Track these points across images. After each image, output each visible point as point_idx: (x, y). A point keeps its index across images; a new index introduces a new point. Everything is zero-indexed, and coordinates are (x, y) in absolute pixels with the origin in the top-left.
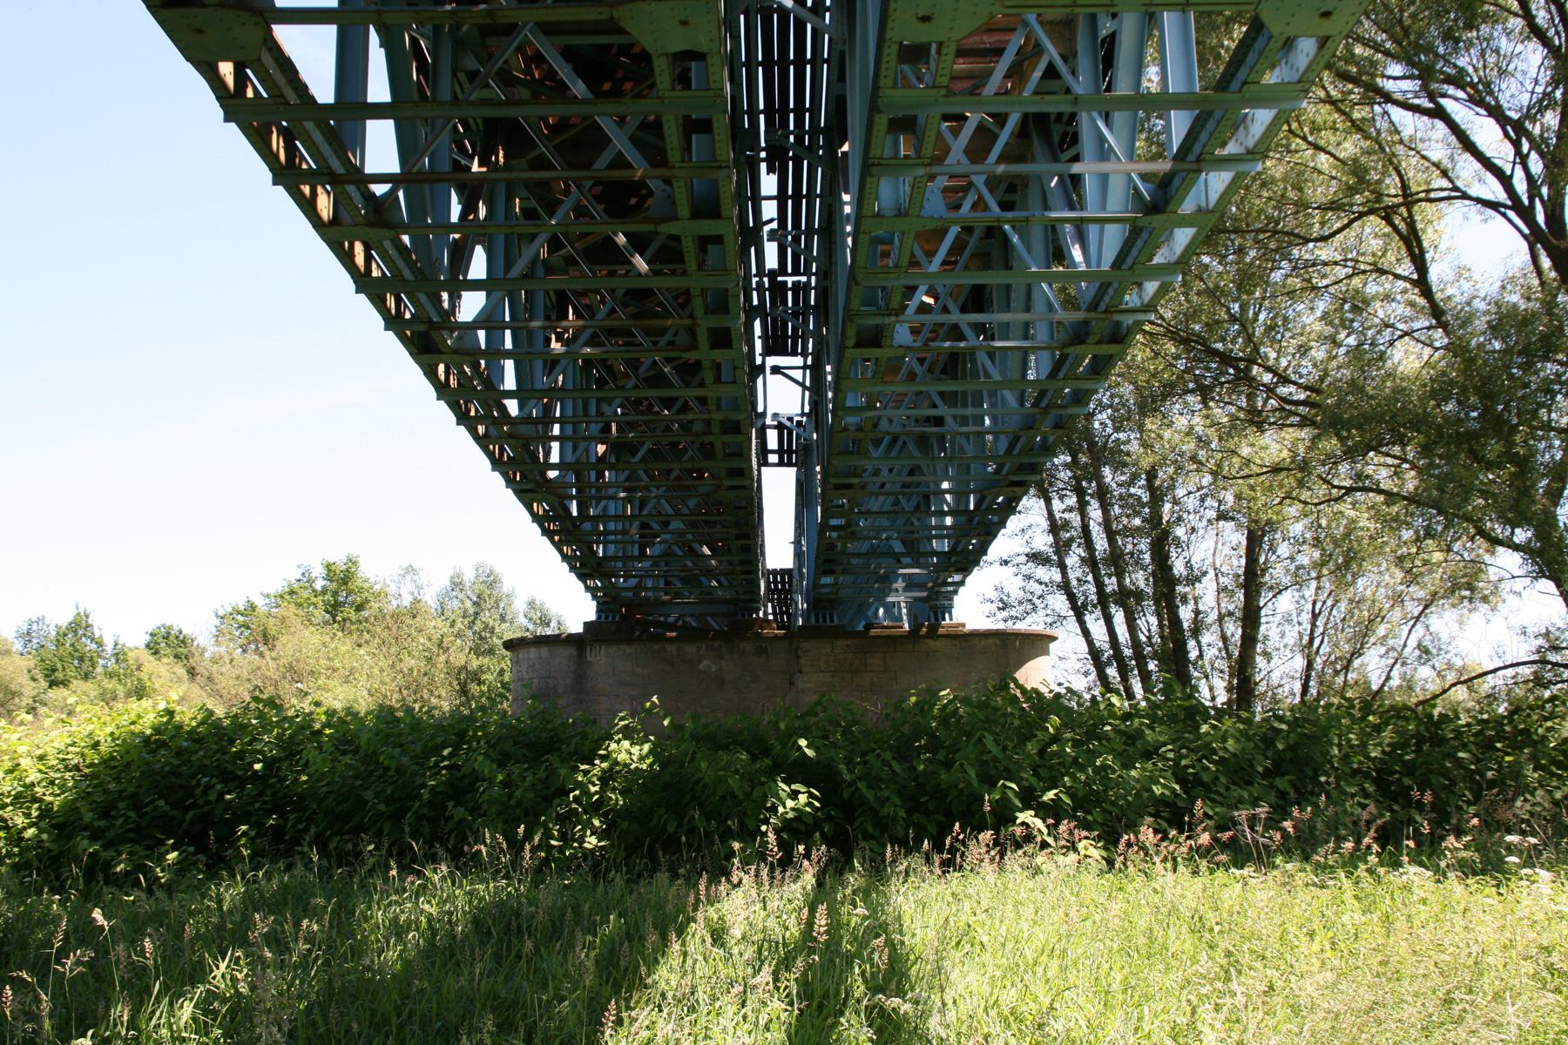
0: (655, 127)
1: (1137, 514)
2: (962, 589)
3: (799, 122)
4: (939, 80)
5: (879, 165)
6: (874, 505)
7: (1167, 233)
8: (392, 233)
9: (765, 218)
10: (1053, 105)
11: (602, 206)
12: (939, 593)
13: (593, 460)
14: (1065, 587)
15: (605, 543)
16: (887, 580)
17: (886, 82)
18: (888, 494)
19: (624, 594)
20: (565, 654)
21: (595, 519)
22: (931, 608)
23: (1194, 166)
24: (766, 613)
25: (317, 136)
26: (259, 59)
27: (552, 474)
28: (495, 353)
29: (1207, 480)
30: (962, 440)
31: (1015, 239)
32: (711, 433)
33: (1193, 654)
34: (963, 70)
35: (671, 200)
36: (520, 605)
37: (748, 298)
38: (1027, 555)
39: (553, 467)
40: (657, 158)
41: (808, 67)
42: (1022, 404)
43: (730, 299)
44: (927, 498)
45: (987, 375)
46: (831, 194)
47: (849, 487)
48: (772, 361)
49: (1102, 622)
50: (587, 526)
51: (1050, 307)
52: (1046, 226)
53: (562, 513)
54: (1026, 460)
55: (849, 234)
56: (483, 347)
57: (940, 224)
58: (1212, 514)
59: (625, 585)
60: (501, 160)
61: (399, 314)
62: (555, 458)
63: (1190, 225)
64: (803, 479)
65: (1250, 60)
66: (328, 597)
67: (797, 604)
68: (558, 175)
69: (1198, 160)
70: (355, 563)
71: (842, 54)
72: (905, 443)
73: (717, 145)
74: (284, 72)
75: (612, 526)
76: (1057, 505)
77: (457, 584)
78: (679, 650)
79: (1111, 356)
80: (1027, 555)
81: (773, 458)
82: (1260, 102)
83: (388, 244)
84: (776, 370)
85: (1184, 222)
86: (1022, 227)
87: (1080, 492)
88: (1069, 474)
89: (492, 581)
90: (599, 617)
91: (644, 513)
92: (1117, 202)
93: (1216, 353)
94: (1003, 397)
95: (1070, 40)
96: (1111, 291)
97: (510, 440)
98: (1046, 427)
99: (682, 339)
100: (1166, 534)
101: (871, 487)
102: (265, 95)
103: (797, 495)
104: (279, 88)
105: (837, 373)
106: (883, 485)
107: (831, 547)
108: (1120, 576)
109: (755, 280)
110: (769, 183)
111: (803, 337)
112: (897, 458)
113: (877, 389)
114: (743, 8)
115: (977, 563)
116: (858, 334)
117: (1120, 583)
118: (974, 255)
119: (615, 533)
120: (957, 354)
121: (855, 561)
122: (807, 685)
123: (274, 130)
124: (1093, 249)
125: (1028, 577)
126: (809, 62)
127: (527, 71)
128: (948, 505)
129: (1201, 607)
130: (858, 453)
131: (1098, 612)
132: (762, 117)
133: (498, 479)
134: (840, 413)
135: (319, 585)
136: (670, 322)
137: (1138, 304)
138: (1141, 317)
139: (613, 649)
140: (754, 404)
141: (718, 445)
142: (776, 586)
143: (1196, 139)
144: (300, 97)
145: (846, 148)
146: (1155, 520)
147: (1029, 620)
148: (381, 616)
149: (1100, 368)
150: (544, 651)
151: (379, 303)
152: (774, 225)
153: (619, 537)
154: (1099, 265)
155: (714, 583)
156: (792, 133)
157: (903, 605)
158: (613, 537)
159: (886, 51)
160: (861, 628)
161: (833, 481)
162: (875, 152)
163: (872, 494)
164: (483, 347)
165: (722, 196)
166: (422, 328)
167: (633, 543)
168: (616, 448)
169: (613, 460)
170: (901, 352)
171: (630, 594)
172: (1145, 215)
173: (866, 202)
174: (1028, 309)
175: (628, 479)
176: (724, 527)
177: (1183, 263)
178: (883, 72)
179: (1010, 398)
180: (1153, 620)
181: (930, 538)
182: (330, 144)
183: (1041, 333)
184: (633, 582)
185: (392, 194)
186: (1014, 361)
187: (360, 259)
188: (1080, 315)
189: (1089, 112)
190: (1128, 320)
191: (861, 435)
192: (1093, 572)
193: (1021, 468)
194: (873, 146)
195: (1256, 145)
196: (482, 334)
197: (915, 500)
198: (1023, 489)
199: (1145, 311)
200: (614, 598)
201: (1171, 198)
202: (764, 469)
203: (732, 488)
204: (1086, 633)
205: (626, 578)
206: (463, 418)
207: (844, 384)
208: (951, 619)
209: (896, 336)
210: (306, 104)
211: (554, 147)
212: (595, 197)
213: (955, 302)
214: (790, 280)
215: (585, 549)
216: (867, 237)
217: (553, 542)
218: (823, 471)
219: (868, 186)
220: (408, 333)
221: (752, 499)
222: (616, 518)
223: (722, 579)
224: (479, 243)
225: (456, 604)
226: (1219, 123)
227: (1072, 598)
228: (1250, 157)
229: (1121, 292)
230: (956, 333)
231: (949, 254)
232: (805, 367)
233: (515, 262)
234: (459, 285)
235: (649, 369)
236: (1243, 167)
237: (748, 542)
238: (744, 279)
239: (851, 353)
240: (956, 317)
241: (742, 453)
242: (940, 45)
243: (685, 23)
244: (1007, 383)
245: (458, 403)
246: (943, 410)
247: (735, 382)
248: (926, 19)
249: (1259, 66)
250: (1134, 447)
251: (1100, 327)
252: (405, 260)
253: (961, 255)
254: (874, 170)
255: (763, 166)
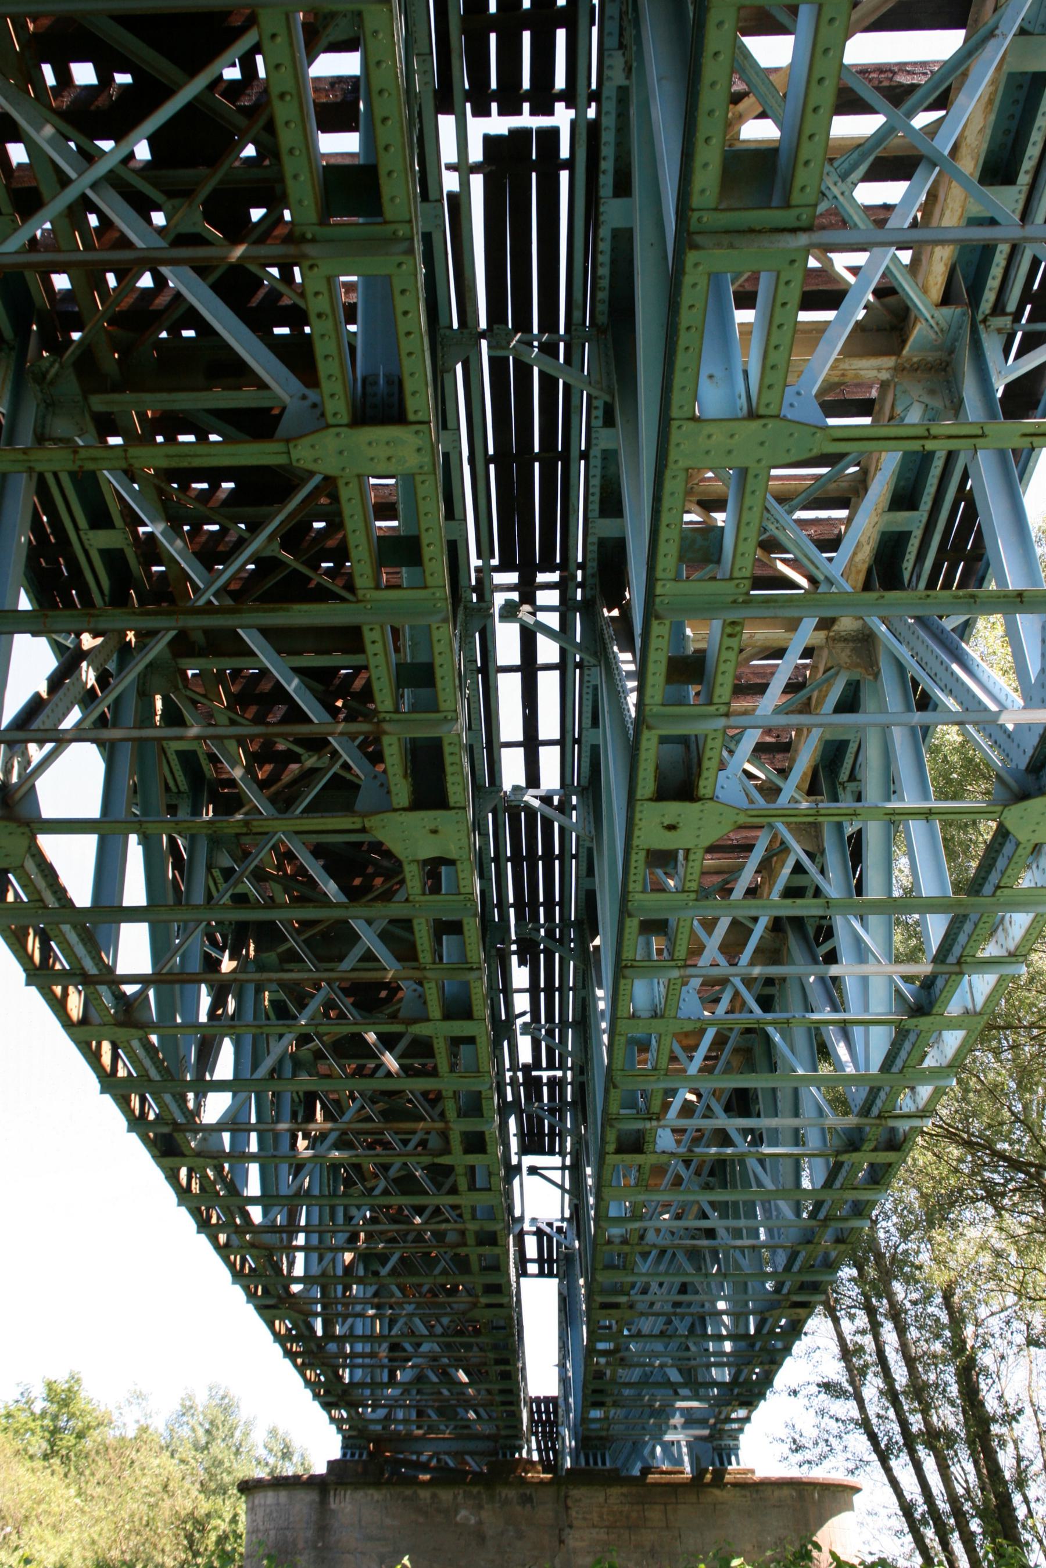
0: (406, 924)
1: (938, 1336)
2: (747, 1427)
3: (550, 916)
4: (688, 884)
5: (632, 966)
6: (646, 1325)
7: (936, 1034)
8: (141, 1033)
9: (517, 1011)
10: (805, 908)
11: (352, 999)
12: (722, 1430)
13: (340, 1272)
14: (865, 1424)
15: (352, 1367)
16: (664, 1413)
17: (634, 886)
18: (657, 1315)
19: (372, 1427)
20: (305, 1500)
21: (341, 1340)
22: (714, 1449)
23: (956, 969)
24: (529, 1451)
25: (72, 937)
26: (22, 866)
27: (296, 1288)
28: (240, 1157)
29: (1011, 1299)
30: (738, 1254)
31: (777, 1038)
32: (465, 1245)
33: (1021, 1512)
34: (710, 866)
35: (422, 999)
36: (259, 1437)
37: (502, 1095)
38: (819, 1385)
39: (297, 1280)
40: (406, 953)
41: (557, 862)
42: (798, 1215)
43: (484, 1102)
44: (703, 1317)
45: (760, 1184)
46: (584, 987)
47: (616, 1306)
48: (529, 1161)
49: (910, 1468)
50: (332, 1347)
51: (821, 1112)
52: (809, 1029)
53: (306, 1333)
54: (808, 1278)
55: (604, 1032)
56: (227, 1150)
57: (698, 1025)
58: (1020, 1339)
59: (374, 1416)
60: (252, 953)
61: (143, 1114)
62: (299, 1270)
63: (959, 1027)
64: (565, 1292)
65: (1000, 863)
66: (47, 1422)
67: (563, 1439)
68: (306, 972)
69: (959, 963)
70: (77, 1381)
71: (590, 851)
72: (674, 1255)
73: (468, 948)
74: (45, 877)
75: (359, 1347)
76: (846, 1325)
77: (188, 1409)
78: (434, 1496)
79: (890, 1165)
80: (819, 1385)
81: (533, 1268)
82: (1020, 903)
83: (135, 1044)
84: (533, 1170)
85: (953, 1024)
86: (785, 1028)
87: (871, 1312)
88: (857, 1290)
89: (226, 1406)
90: (344, 1455)
91: (393, 1333)
92: (880, 1005)
93: (1001, 1156)
94: (777, 1208)
95: (817, 837)
96: (882, 1095)
97: (255, 1251)
98: (826, 1240)
99: (434, 1142)
100: (972, 1361)
101: (641, 1307)
102: (25, 899)
103: (560, 1310)
104: (39, 892)
105: (598, 1176)
106: (652, 1304)
107: (599, 1375)
108: (925, 1412)
109: (508, 1074)
110: (520, 976)
111: (560, 1135)
112: (667, 1273)
113: (641, 1198)
114: (492, 806)
115: (762, 1396)
116: (619, 1139)
117: (927, 1422)
118: (736, 1051)
119: (362, 1355)
120: (725, 1161)
121: (627, 1392)
122: (579, 1544)
123: (31, 931)
124: (859, 1048)
125: (822, 1413)
126: (558, 857)
127: (280, 867)
128: (726, 1327)
129: (1022, 1453)
130: (625, 1268)
131: (905, 1457)
132: (512, 911)
133: (238, 1293)
134: (603, 1224)
135: (37, 1408)
136: (421, 1125)
137: (913, 1109)
138: (916, 1123)
139: (359, 1495)
140: (510, 1209)
141: (473, 1258)
142: (540, 1417)
143: (954, 940)
144: (59, 900)
145: (597, 941)
146: (958, 1346)
147: (827, 1464)
148: (104, 1449)
149: (879, 1177)
150: (283, 1495)
151: (123, 1102)
152: (527, 1018)
153: (367, 1361)
154: (867, 1068)
155: (472, 1415)
156: (542, 926)
157: (683, 1443)
158: (360, 1361)
159: (634, 857)
160: (636, 1472)
161: (599, 1299)
162: (627, 955)
163: (642, 1314)
164: (227, 1150)
165: (474, 997)
166: (166, 1130)
167: (382, 1367)
168: (364, 1257)
169: (361, 1272)
170: (664, 1158)
171: (379, 1427)
172: (911, 1017)
173: (620, 1003)
174: (796, 1114)
175: (376, 1294)
176: (481, 1349)
177: (957, 1065)
178: (632, 878)
179: (786, 1209)
180: (970, 1467)
181: (709, 1365)
182: (85, 945)
183: (813, 1140)
184: (381, 1413)
185: (142, 995)
186: (786, 1168)
187: (106, 1059)
188: (852, 1120)
189: (844, 915)
190: (904, 1126)
191: (626, 1249)
192: (894, 1406)
193: (803, 1287)
194: (625, 949)
195: (1017, 948)
196: (226, 1136)
197: (688, 1320)
198: (807, 1310)
199: (921, 1117)
200: (360, 1431)
201: (936, 1000)
202: (522, 1280)
203: (489, 1306)
204: (894, 1483)
205: (375, 1407)
206: (204, 1225)
207: (606, 1191)
208: (738, 1463)
209: (658, 1140)
210: (63, 907)
211: (304, 941)
212: (342, 990)
213: (718, 1100)
214: (545, 1075)
215: (330, 1374)
216: (623, 1039)
217: (295, 1365)
218: (587, 1285)
219: (622, 987)
220: (151, 1135)
221: (512, 1318)
222: (365, 1338)
223: (481, 1410)
224: (226, 1035)
225: (185, 1432)
226: (976, 925)
227: (873, 1438)
228: (1013, 959)
229: (893, 1095)
230: (723, 1138)
231: (710, 1049)
232: (563, 1168)
233: (264, 1059)
234: (204, 1087)
235: (400, 1169)
236: (1009, 970)
237: (508, 1368)
238: (498, 1073)
239: (612, 1159)
240: (722, 1121)
241: (498, 1267)
242: (687, 851)
243: (435, 832)
244: (781, 1193)
245: (199, 1209)
246: (714, 1221)
247: (490, 1189)
248: (671, 828)
249: (1009, 871)
250: (924, 1257)
251: (874, 1133)
252: (152, 1059)
253: (722, 1051)
254: (627, 972)
255: (514, 959)
